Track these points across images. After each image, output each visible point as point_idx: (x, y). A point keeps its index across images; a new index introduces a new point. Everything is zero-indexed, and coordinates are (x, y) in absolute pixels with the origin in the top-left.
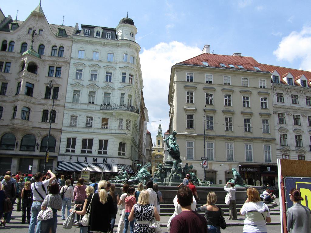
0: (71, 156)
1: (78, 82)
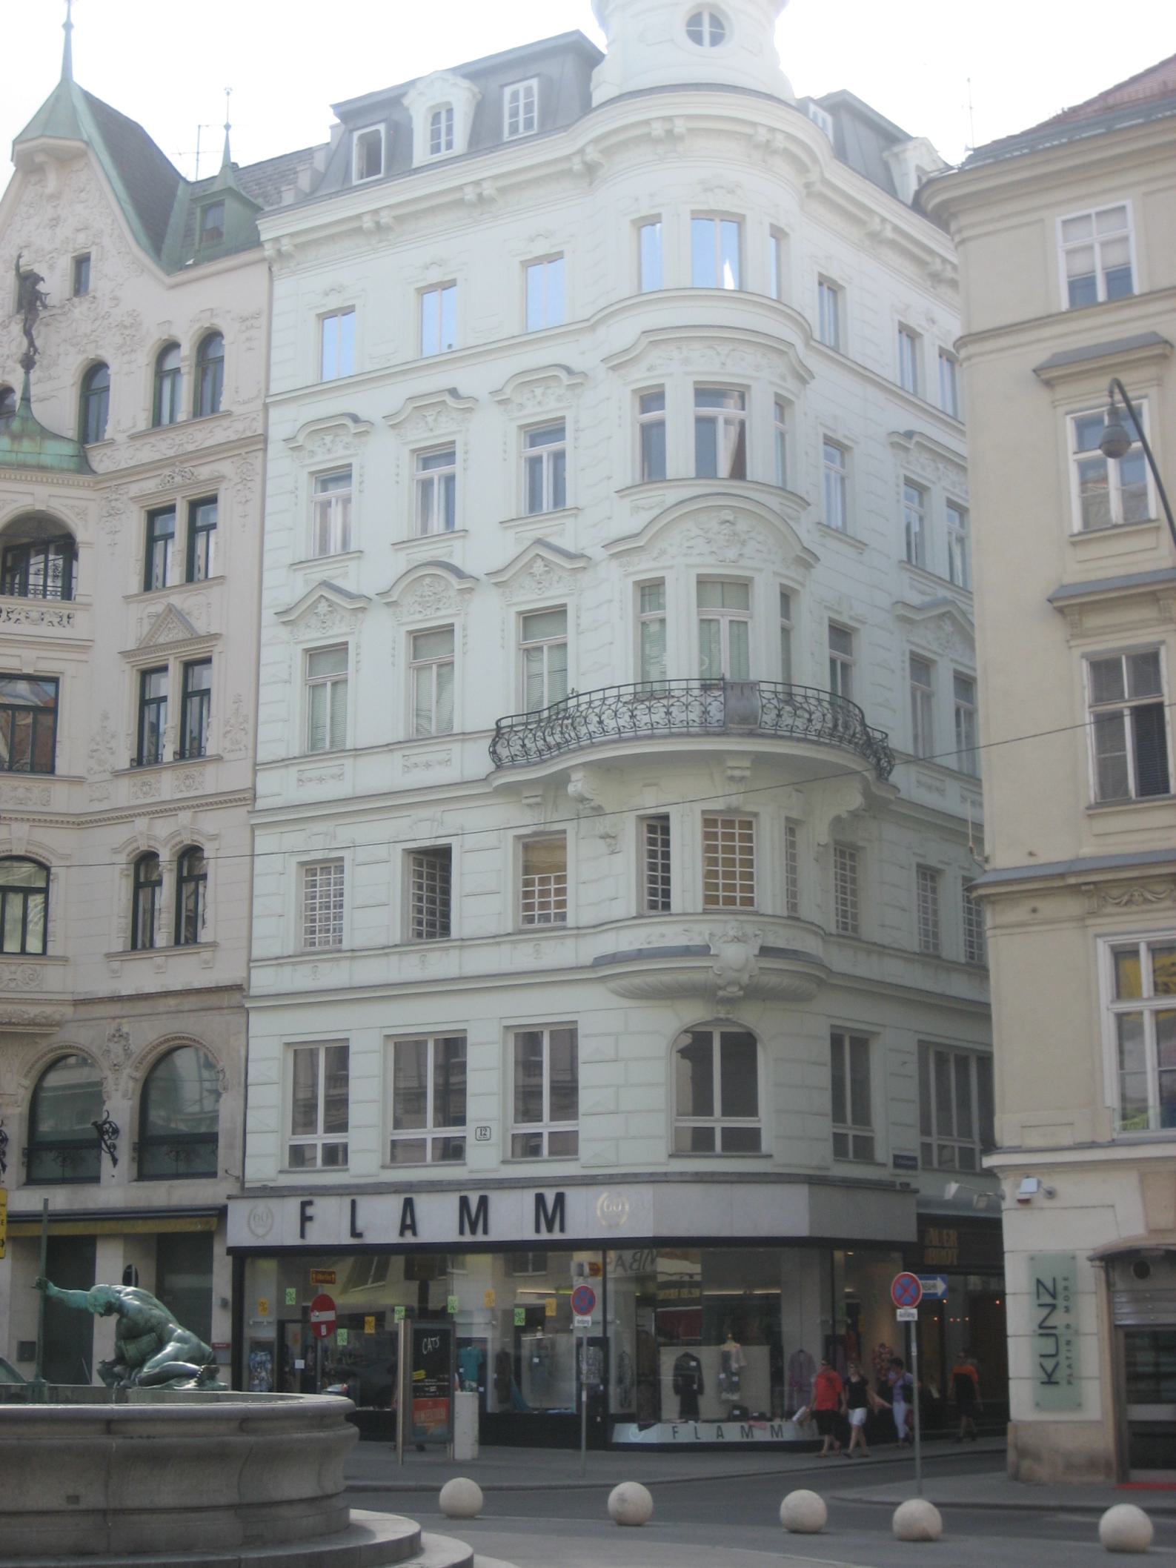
0: (307, 1197)
1: (539, 542)
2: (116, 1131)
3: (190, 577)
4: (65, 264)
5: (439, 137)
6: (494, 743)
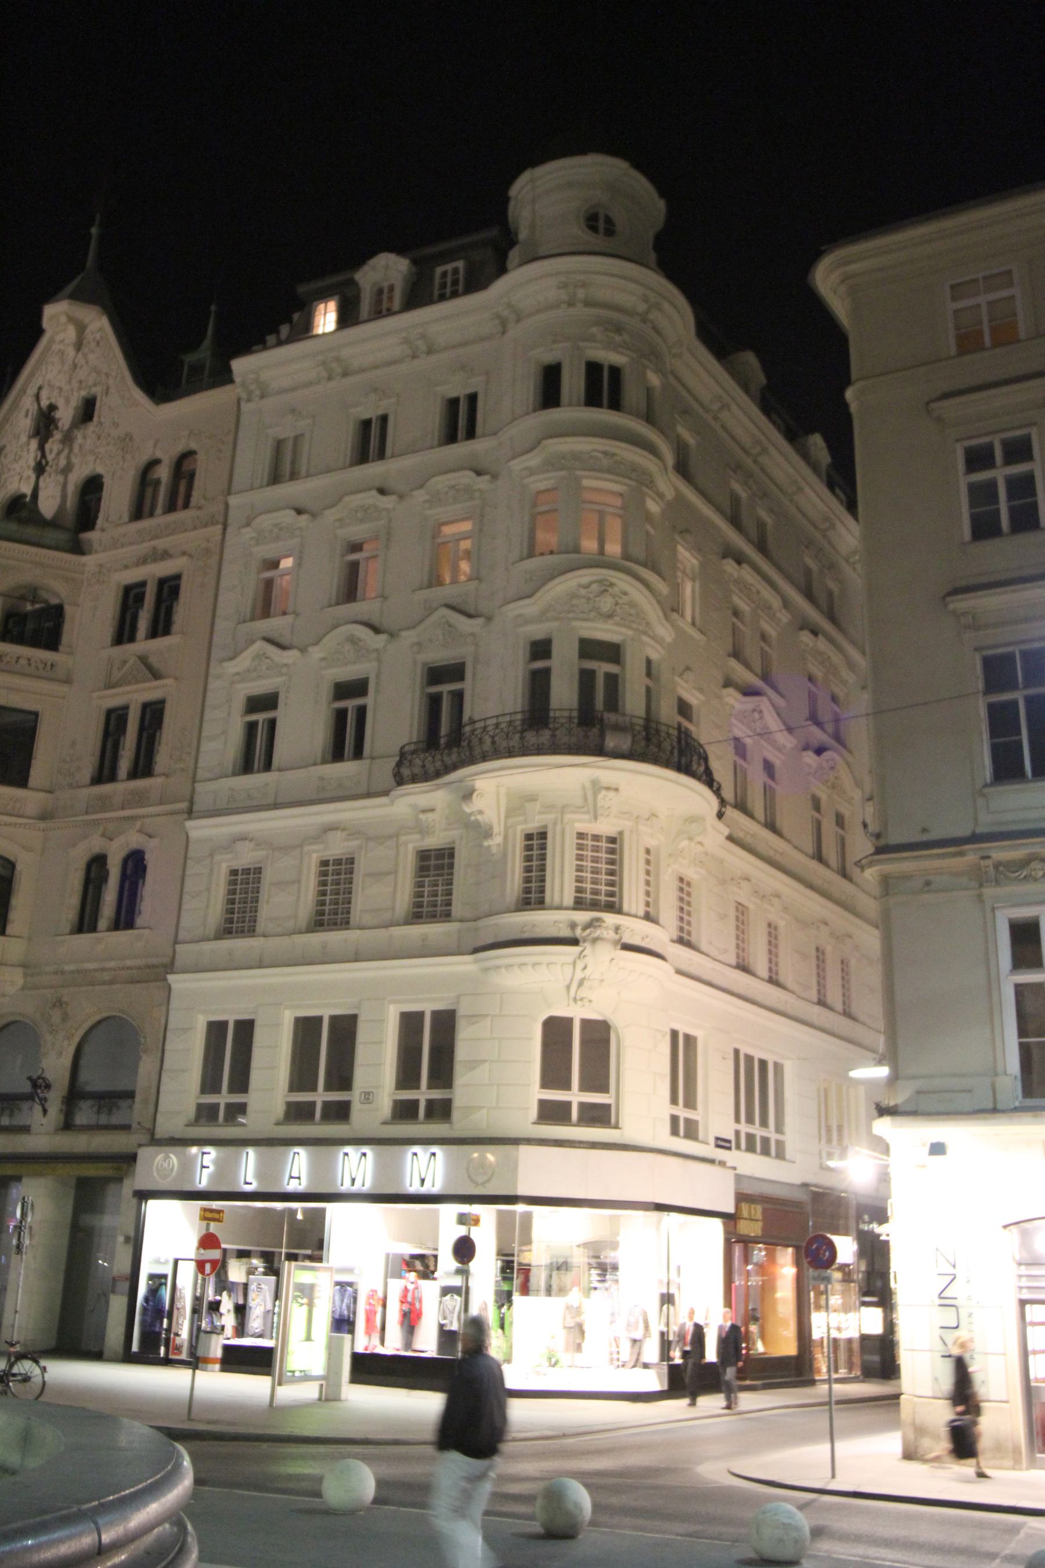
2: (48, 1086)
5: (381, 305)
6: (399, 764)
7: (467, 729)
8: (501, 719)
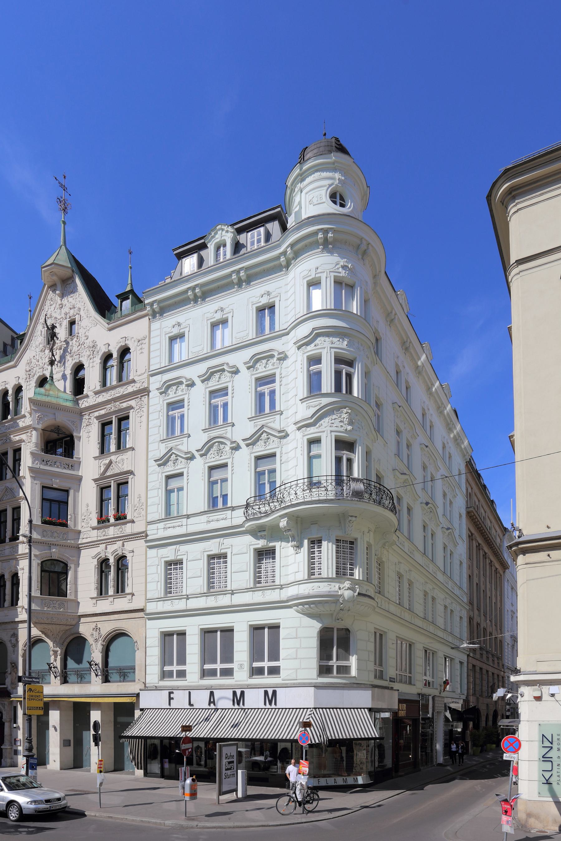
3: (119, 447)
4: (65, 323)
7: (278, 490)
8: (292, 483)
